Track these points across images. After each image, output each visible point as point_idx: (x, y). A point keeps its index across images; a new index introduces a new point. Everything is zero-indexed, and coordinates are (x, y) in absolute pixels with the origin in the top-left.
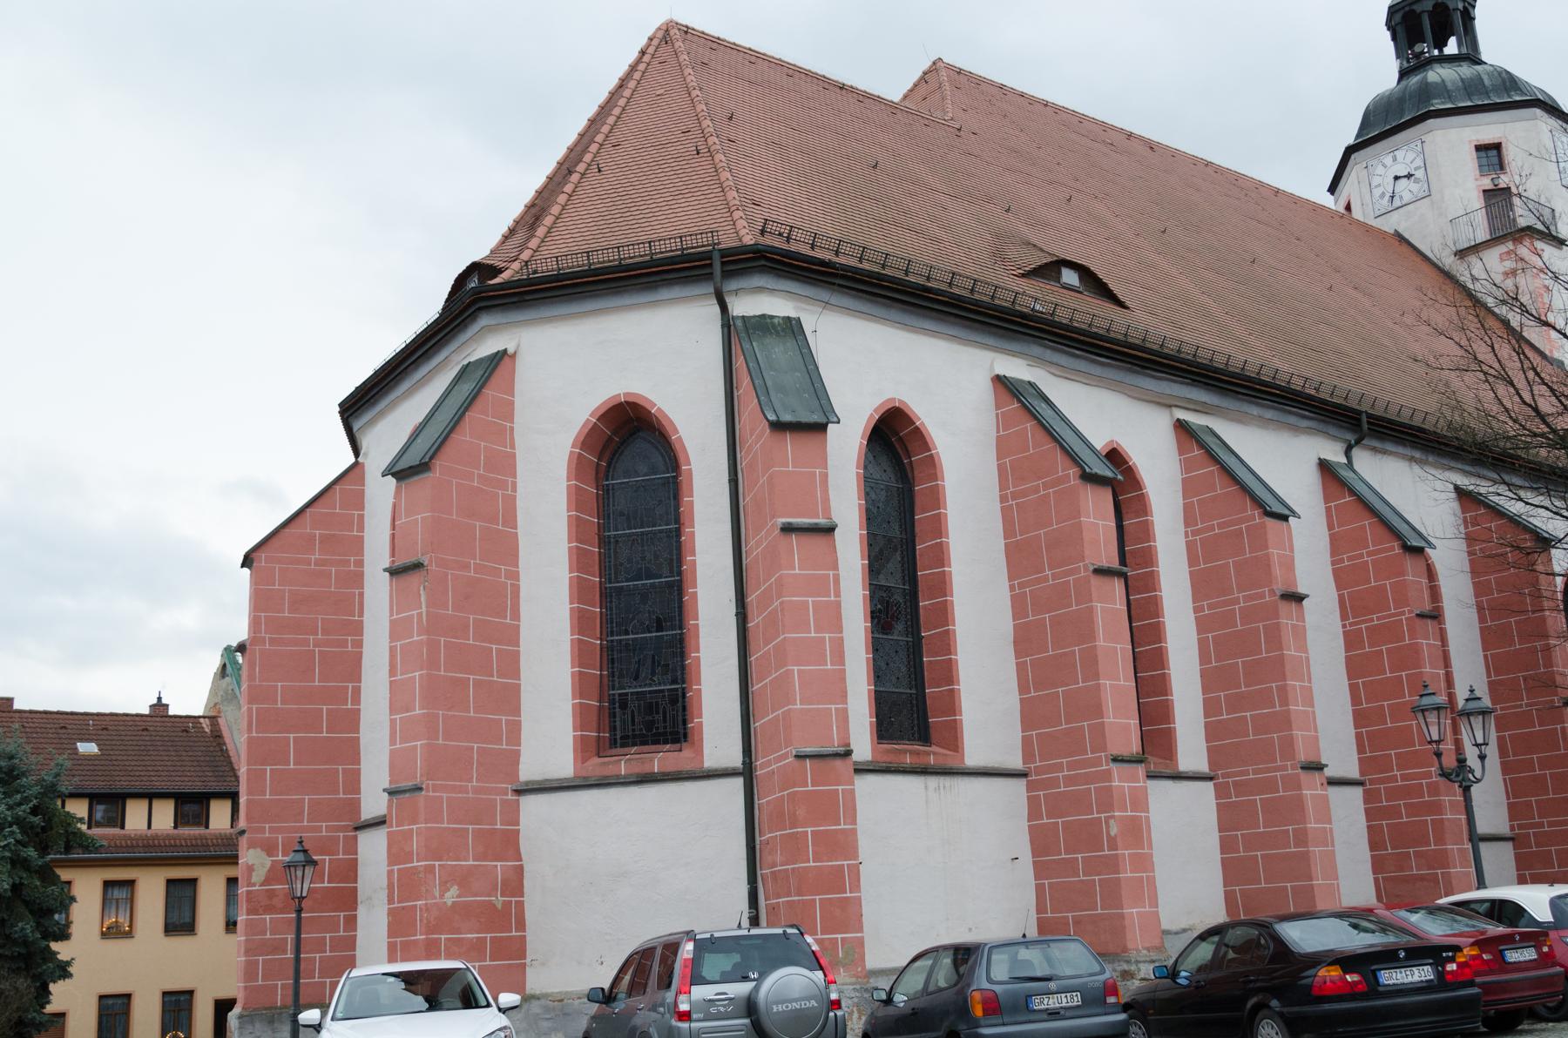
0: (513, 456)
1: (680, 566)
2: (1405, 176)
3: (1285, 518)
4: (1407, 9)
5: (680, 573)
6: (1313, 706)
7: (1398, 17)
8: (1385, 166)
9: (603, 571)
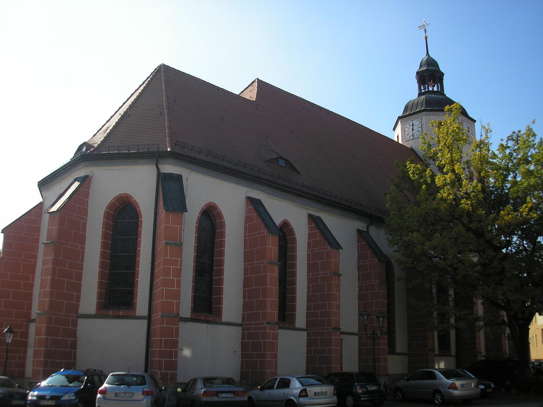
4: (422, 74)
5: (136, 252)
6: (339, 310)
7: (419, 75)
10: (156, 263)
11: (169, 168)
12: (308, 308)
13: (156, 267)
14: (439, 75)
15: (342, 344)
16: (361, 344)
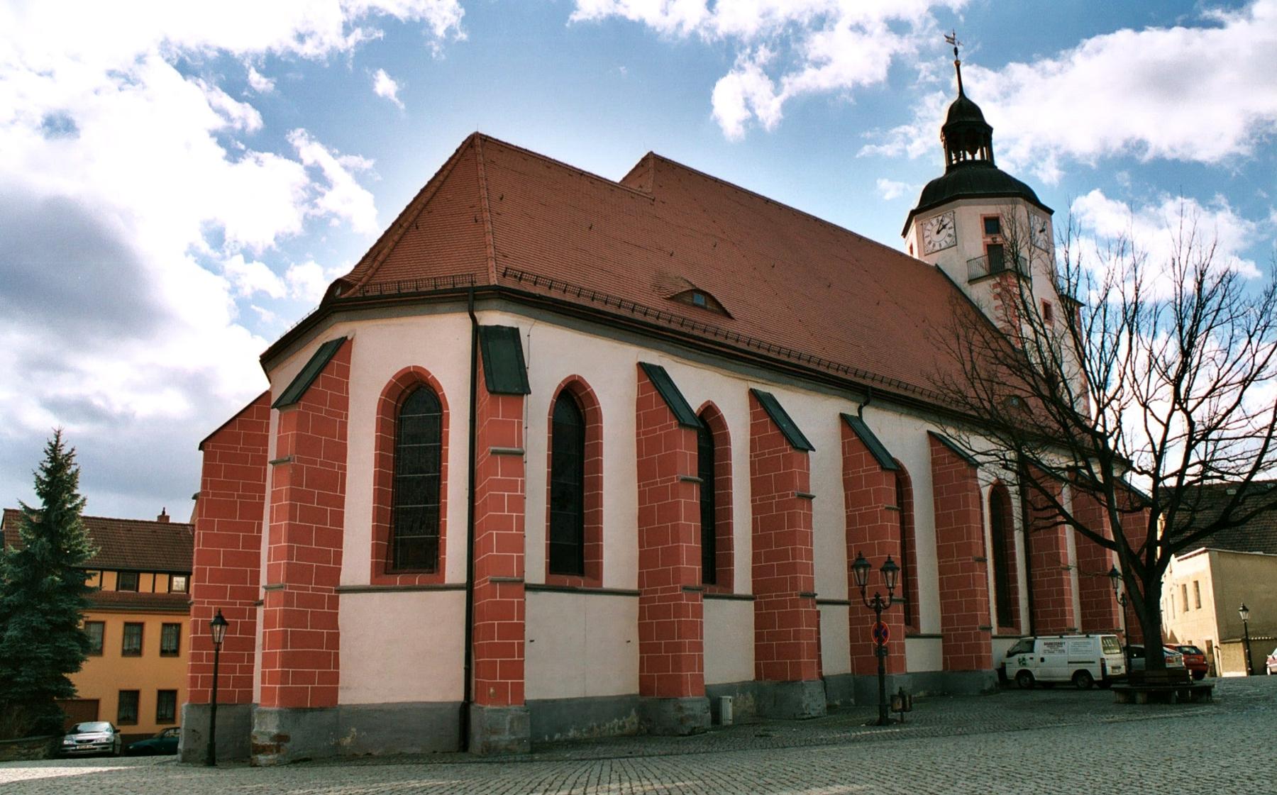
0: (347, 398)
1: (440, 468)
3: (807, 451)
5: (440, 472)
8: (932, 225)
9: (396, 467)
10: (477, 489)
11: (492, 318)
12: (756, 558)
13: (478, 496)
15: (819, 622)
16: (853, 621)
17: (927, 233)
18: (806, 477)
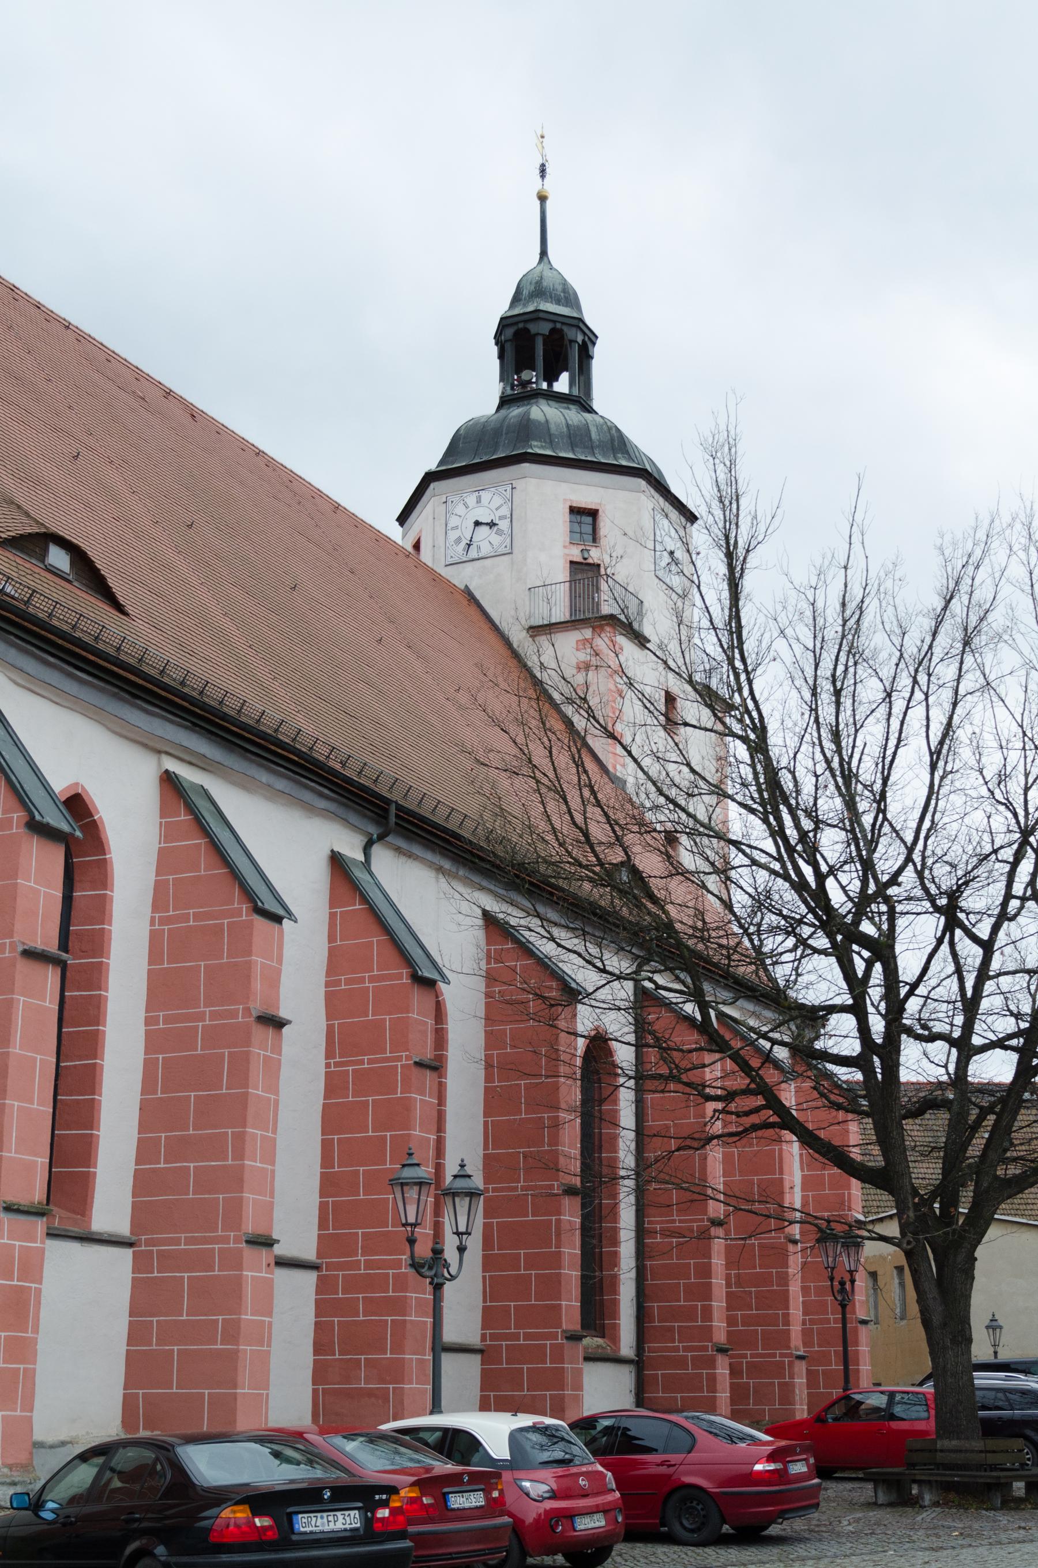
2: (487, 524)
3: (278, 919)
4: (521, 325)
6: (273, 1163)
7: (509, 333)
14: (580, 338)
17: (453, 521)
18: (273, 980)
